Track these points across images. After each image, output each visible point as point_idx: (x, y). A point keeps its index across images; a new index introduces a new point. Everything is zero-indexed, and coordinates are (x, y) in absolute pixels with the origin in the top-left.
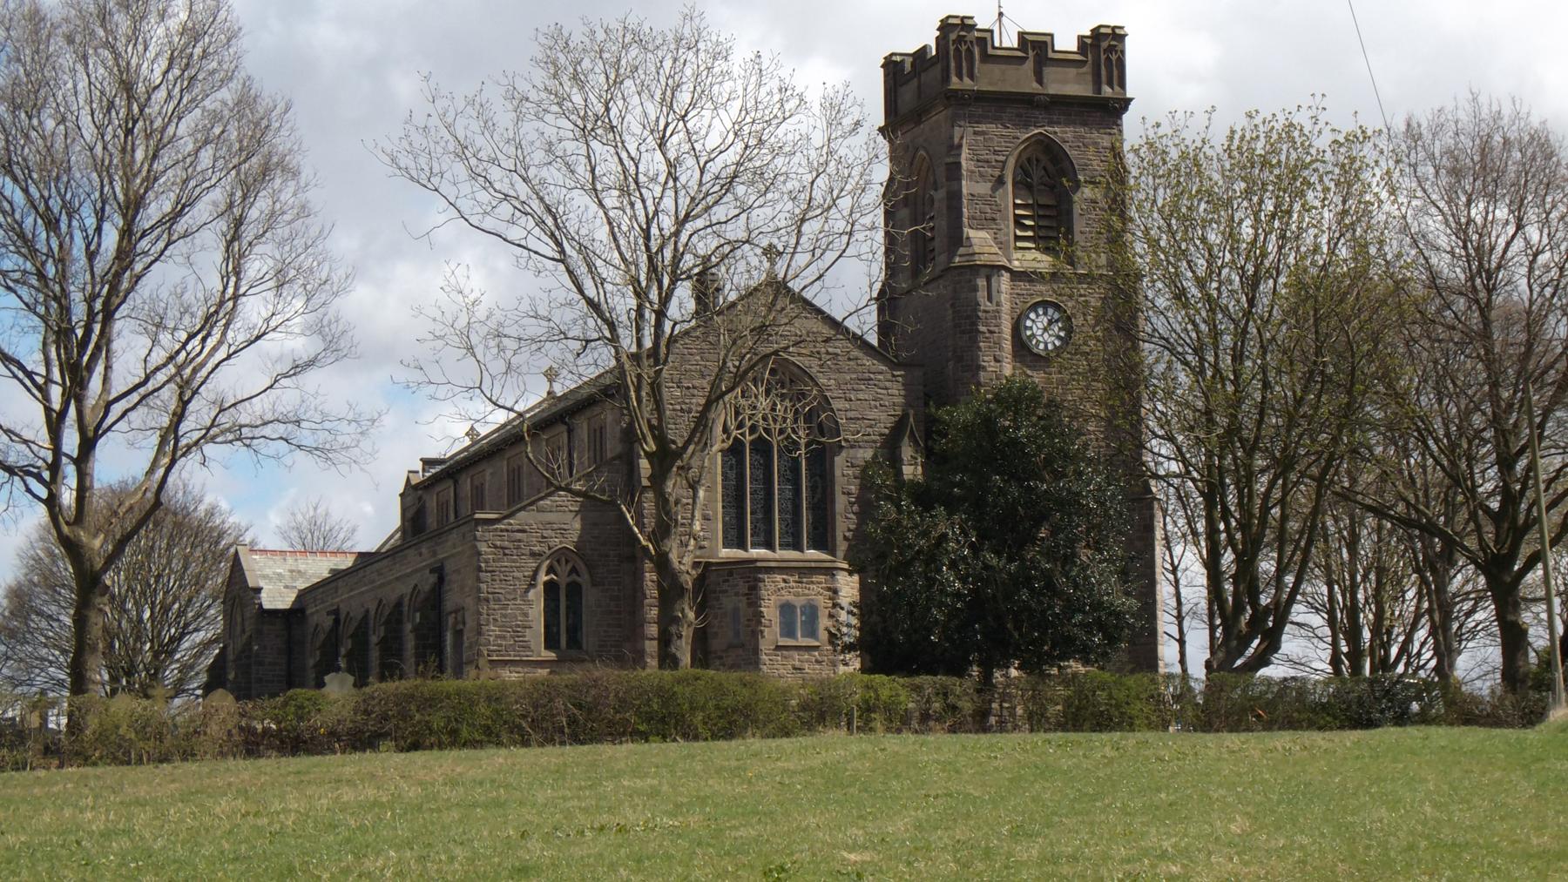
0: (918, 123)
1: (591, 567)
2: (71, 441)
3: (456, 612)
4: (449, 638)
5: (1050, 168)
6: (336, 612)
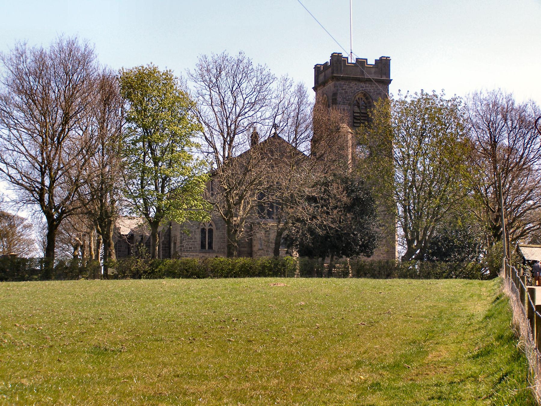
0: (324, 86)
1: (216, 224)
2: (47, 182)
3: (174, 237)
4: (172, 245)
5: (365, 100)
6: (142, 236)
